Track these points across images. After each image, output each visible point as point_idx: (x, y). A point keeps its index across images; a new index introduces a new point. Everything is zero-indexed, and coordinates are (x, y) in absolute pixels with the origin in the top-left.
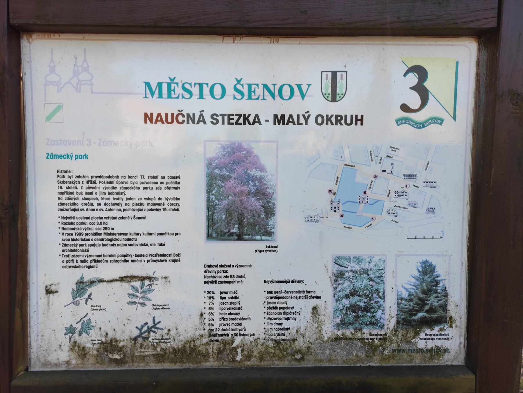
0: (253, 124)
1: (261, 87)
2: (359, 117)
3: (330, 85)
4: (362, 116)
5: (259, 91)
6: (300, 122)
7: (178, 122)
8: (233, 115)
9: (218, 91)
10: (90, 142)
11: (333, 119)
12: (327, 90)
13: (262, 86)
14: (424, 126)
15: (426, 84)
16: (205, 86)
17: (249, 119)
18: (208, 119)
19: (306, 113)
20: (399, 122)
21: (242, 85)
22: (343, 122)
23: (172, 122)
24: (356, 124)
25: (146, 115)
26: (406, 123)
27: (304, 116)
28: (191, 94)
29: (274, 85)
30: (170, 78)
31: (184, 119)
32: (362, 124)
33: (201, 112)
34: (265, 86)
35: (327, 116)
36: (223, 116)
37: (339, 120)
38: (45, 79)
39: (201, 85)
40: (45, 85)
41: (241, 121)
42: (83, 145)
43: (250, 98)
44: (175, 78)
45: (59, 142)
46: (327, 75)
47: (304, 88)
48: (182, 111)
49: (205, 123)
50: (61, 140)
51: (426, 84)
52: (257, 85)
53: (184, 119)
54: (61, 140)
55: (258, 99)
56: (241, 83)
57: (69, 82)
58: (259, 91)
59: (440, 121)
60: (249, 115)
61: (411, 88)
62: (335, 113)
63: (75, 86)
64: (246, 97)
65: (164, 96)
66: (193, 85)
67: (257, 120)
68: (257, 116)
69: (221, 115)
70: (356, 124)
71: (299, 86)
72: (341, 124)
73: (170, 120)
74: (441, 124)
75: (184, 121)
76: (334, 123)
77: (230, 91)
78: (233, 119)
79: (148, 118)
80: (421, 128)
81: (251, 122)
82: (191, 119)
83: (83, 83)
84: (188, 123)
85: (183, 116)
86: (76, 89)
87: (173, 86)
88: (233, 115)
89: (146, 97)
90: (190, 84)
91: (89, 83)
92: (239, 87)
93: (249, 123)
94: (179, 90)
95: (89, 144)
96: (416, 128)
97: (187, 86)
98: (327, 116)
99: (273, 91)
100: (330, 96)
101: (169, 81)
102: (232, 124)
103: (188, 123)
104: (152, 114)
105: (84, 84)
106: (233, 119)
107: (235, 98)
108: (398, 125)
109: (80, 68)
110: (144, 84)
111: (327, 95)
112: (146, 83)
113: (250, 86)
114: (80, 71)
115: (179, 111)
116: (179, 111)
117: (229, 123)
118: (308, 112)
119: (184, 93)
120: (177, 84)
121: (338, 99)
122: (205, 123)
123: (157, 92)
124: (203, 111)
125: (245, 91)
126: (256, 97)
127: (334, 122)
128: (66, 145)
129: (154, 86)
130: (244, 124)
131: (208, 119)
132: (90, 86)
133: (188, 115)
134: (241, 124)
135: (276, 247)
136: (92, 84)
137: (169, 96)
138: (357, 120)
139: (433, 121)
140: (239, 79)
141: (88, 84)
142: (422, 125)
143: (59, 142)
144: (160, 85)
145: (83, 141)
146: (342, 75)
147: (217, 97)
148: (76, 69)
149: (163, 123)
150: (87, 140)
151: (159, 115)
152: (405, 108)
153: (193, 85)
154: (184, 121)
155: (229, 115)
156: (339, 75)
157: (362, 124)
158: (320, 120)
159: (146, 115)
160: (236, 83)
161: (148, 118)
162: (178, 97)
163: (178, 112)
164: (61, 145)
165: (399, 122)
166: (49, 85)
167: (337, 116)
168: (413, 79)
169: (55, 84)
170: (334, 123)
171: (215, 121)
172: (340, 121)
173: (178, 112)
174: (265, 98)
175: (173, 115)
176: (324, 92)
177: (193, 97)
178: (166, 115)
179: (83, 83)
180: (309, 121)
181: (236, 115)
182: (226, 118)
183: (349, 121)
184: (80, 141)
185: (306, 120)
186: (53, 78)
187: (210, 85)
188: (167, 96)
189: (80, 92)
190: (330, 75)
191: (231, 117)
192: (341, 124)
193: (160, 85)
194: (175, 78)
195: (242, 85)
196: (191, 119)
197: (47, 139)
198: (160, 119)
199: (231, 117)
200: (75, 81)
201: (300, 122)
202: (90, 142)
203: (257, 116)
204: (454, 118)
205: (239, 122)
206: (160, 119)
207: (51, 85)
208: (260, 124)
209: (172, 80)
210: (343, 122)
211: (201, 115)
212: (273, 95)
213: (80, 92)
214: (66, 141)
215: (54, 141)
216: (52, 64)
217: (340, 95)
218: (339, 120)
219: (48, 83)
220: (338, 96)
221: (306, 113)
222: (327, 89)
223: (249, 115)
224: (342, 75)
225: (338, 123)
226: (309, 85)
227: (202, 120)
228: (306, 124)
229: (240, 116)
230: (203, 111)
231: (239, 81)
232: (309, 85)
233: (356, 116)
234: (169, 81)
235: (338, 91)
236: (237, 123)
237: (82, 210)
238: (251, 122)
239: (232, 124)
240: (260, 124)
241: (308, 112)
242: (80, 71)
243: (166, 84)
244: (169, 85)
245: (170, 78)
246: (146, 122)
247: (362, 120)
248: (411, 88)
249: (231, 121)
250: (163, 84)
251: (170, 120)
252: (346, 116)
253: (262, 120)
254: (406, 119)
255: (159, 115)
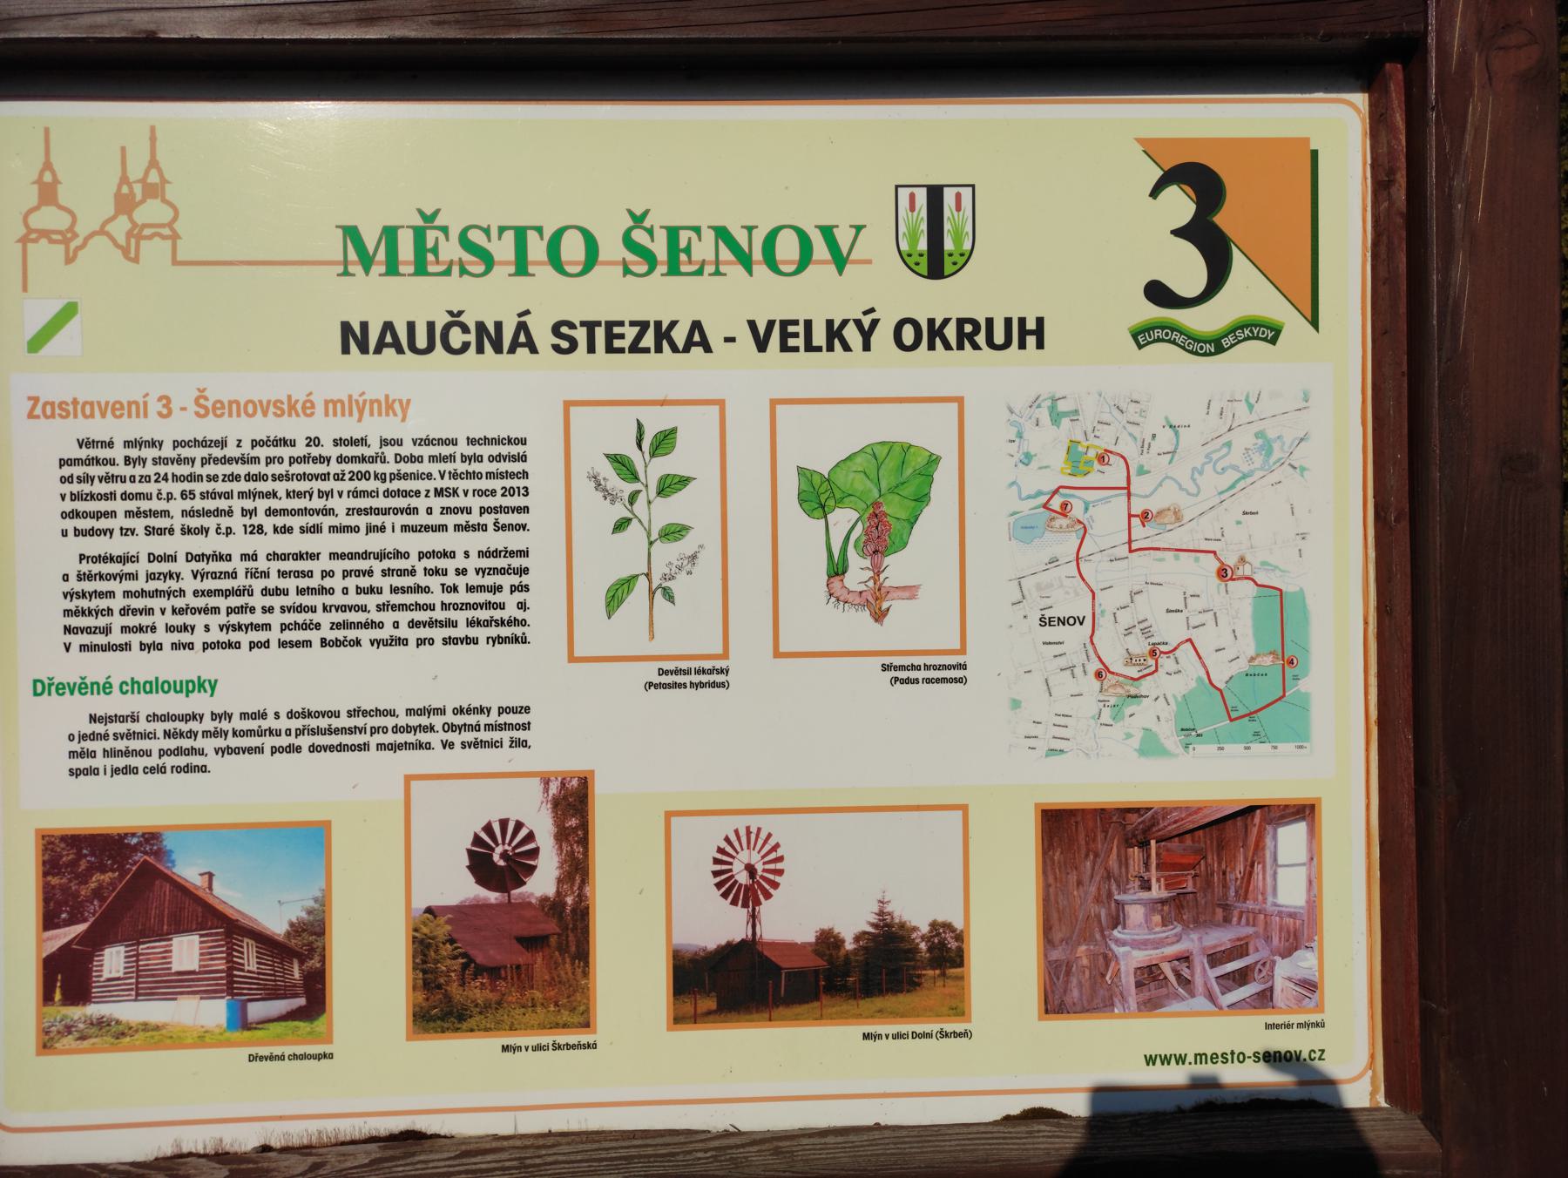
0: (687, 349)
1: (708, 236)
2: (1031, 325)
3: (924, 227)
4: (1040, 321)
5: (704, 249)
6: (815, 343)
7: (448, 348)
8: (621, 324)
9: (573, 248)
10: (167, 406)
11: (951, 332)
12: (913, 240)
13: (664, 231)
14: (1220, 349)
15: (1220, 219)
16: (532, 236)
17: (673, 334)
18: (543, 338)
19: (865, 313)
20: (1143, 335)
21: (650, 232)
22: (981, 339)
23: (430, 348)
24: (1022, 346)
25: (346, 328)
26: (1163, 340)
27: (858, 323)
28: (488, 261)
29: (750, 229)
30: (420, 211)
31: (467, 338)
32: (1040, 345)
33: (520, 315)
34: (722, 234)
35: (931, 322)
36: (591, 326)
37: (969, 333)
38: (26, 225)
39: (521, 234)
40: (24, 241)
41: (648, 340)
42: (146, 415)
43: (674, 270)
44: (437, 212)
45: (71, 408)
46: (912, 196)
47: (844, 238)
48: (460, 313)
49: (534, 350)
50: (75, 402)
51: (1220, 219)
52: (697, 230)
53: (467, 338)
54: (75, 402)
55: (699, 272)
56: (647, 224)
57: (102, 232)
58: (704, 249)
59: (1271, 332)
60: (673, 324)
61: (1176, 233)
62: (955, 314)
63: (122, 241)
64: (662, 269)
65: (402, 269)
66: (494, 233)
67: (698, 338)
68: (696, 325)
69: (583, 324)
70: (1022, 346)
71: (828, 232)
72: (976, 347)
73: (421, 343)
74: (1273, 341)
75: (466, 346)
76: (954, 345)
77: (612, 248)
78: (622, 336)
79: (353, 337)
80: (1211, 354)
81: (681, 346)
82: (489, 338)
83: (147, 232)
84: (480, 350)
85: (465, 330)
86: (125, 251)
87: (431, 236)
88: (621, 324)
89: (346, 273)
90: (487, 231)
91: (166, 231)
92: (639, 236)
93: (675, 349)
94: (451, 250)
95: (165, 411)
96: (1196, 353)
97: (476, 237)
98: (931, 322)
99: (745, 246)
100: (924, 261)
101: (419, 222)
102: (621, 350)
103: (480, 350)
104: (364, 326)
105: (150, 237)
106: (622, 336)
107: (627, 271)
108: (1140, 347)
109: (138, 189)
110: (340, 231)
111: (916, 258)
112: (344, 228)
113: (673, 233)
114: (139, 197)
115: (451, 313)
116: (451, 313)
117: (610, 349)
118: (872, 310)
119: (467, 257)
120: (445, 230)
121: (948, 269)
122: (534, 350)
123: (381, 256)
124: (527, 312)
125: (660, 248)
126: (694, 268)
127: (953, 340)
128: (92, 416)
129: (370, 239)
130: (659, 349)
131: (543, 338)
132: (169, 242)
133: (481, 327)
134: (647, 350)
135: (524, 553)
136: (175, 237)
137: (421, 269)
138: (1024, 332)
139: (1247, 332)
140: (429, 212)
141: (164, 237)
142: (1216, 345)
143: (71, 408)
144: (390, 233)
145: (145, 403)
146: (958, 196)
147: (570, 269)
148: (125, 190)
149: (400, 351)
150: (160, 399)
151: (388, 326)
152: (1158, 293)
153: (494, 233)
154: (466, 346)
155: (610, 325)
156: (949, 196)
157: (1040, 345)
158: (908, 335)
159: (346, 328)
160: (631, 223)
161: (353, 337)
162: (447, 273)
163: (450, 319)
164: (76, 416)
165: (1143, 335)
166: (35, 241)
167: (961, 322)
168: (1180, 205)
169: (58, 237)
170: (954, 345)
171: (565, 345)
172: (971, 337)
173: (450, 319)
174: (723, 269)
175: (431, 326)
176: (904, 247)
177: (496, 269)
178: (411, 327)
179: (147, 232)
180: (875, 339)
181: (632, 324)
182: (600, 333)
183: (999, 338)
184: (136, 403)
185: (867, 335)
186: (49, 218)
187: (547, 234)
188: (411, 269)
189: (136, 260)
190: (922, 196)
191: (616, 330)
192: (976, 347)
193: (390, 233)
194: (437, 212)
195: (650, 232)
196: (489, 338)
197: (30, 398)
198: (390, 339)
199: (616, 330)
200: (120, 227)
201: (815, 343)
202: (167, 406)
203: (696, 325)
204: (1314, 323)
205: (642, 344)
206: (390, 339)
207: (44, 241)
208: (708, 349)
209: (429, 218)
210: (981, 339)
211: (522, 327)
212: (745, 260)
213: (136, 260)
214: (92, 404)
215: (52, 404)
216: (48, 177)
217: (956, 258)
218: (969, 333)
219: (33, 236)
220: (947, 261)
221: (865, 313)
222: (913, 240)
223: (673, 324)
224: (958, 196)
225: (966, 343)
226: (859, 229)
227: (524, 339)
228: (867, 347)
229: (643, 326)
230: (527, 312)
231: (638, 220)
232: (859, 229)
233: (1022, 321)
234: (419, 222)
235: (949, 245)
236: (635, 348)
237: (127, 532)
238: (681, 346)
239: (621, 350)
240: (708, 349)
241: (872, 310)
242: (139, 197)
243: (410, 232)
244: (419, 234)
245: (420, 211)
246: (346, 350)
247: (1039, 332)
248: (1176, 233)
249: (617, 343)
250: (400, 231)
251: (421, 343)
252: (990, 322)
253: (715, 340)
254: (1163, 328)
255: (388, 326)
